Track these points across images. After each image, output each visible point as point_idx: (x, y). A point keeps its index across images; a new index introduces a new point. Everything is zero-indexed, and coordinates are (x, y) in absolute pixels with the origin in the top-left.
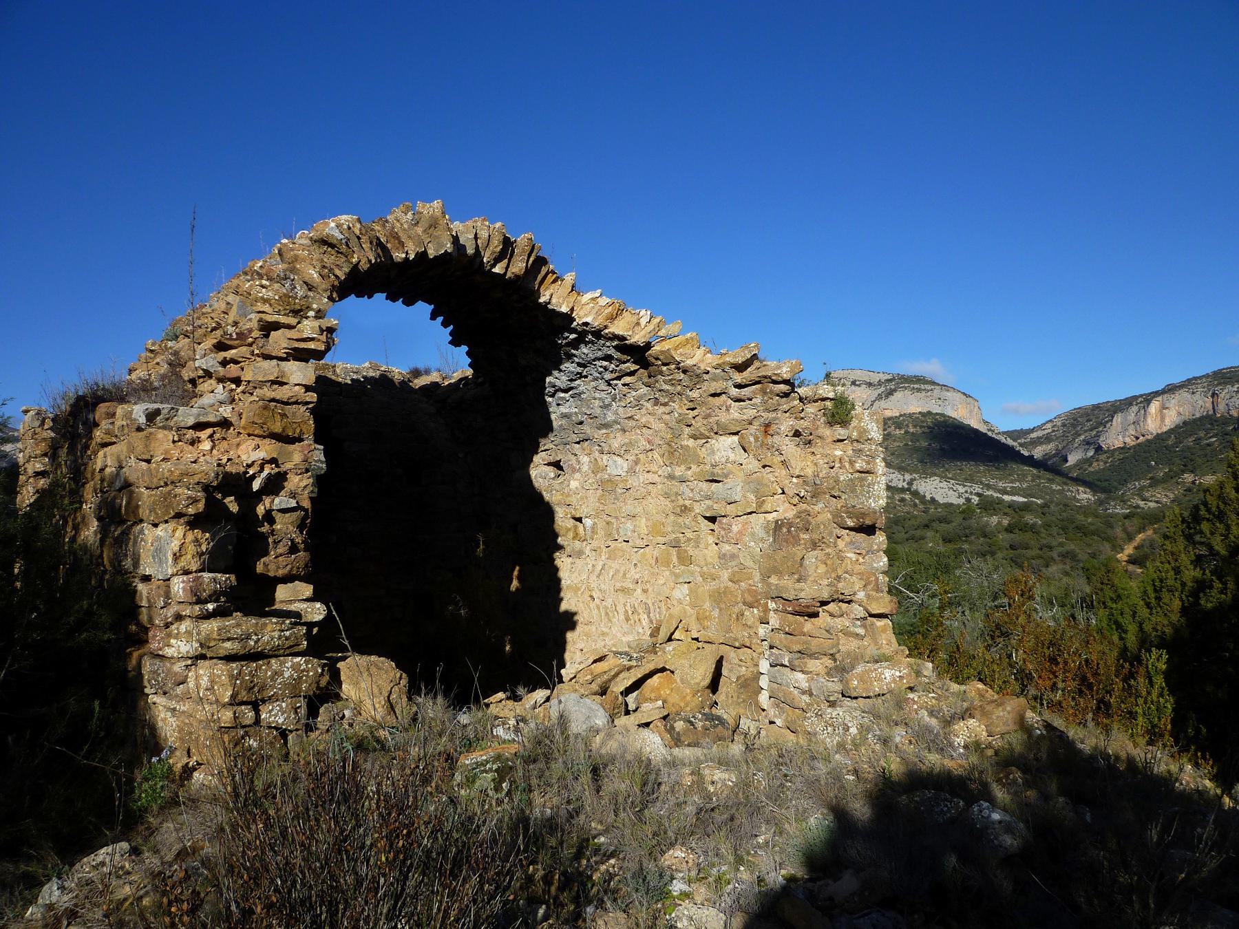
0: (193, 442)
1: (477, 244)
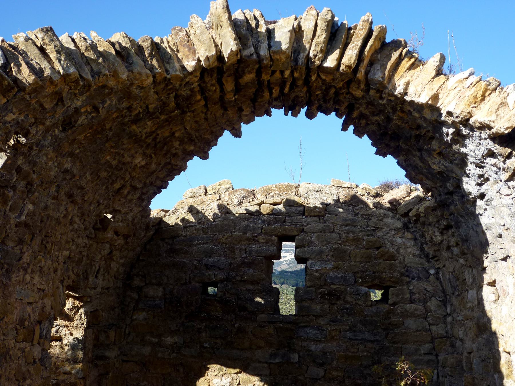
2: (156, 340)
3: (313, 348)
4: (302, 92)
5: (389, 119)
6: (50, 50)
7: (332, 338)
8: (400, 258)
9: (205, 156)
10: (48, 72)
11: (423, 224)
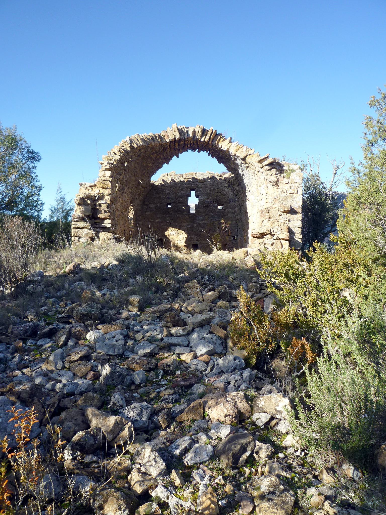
0: (88, 190)
1: (77, 360)
2: (153, 221)
3: (200, 222)
4: (196, 146)
5: (219, 154)
6: (139, 139)
7: (206, 219)
8: (227, 195)
9: (168, 163)
10: (139, 145)
11: (234, 185)
